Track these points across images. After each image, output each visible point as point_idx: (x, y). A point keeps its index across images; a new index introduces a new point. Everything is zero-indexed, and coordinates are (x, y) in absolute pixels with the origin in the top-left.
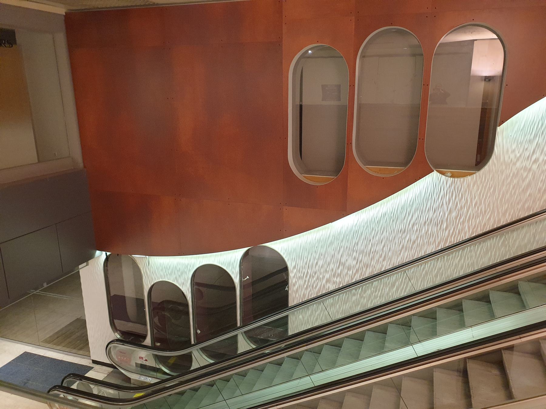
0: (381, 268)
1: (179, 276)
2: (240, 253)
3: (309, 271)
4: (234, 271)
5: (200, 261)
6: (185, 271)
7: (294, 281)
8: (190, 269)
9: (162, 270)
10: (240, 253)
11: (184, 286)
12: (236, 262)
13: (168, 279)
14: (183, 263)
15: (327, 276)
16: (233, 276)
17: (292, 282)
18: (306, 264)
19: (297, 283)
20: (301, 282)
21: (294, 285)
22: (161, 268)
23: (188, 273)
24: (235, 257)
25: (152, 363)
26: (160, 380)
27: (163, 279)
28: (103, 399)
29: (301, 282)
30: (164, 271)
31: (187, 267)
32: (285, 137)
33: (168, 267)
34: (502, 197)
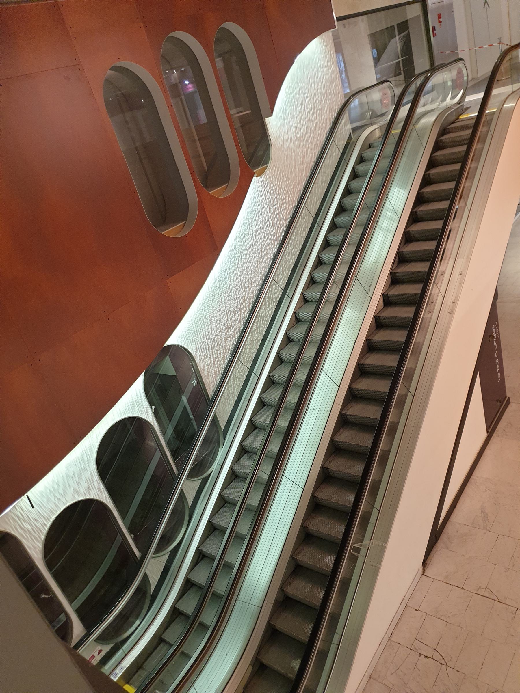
0: (289, 219)
1: (78, 483)
2: (139, 384)
3: (209, 343)
4: (142, 409)
5: (97, 435)
6: (83, 467)
7: (202, 366)
8: (88, 457)
9: (48, 500)
10: (139, 384)
11: (90, 491)
12: (139, 397)
13: (64, 504)
14: (75, 459)
15: (223, 335)
16: (105, 501)
17: (201, 368)
18: (204, 337)
19: (206, 366)
20: (208, 361)
21: (204, 370)
22: (49, 491)
23: (88, 468)
24: (132, 397)
25: (164, 558)
26: (410, 104)
27: (57, 512)
28: (287, 437)
29: (208, 361)
30: (52, 499)
31: (83, 459)
32: (105, 310)
33: (56, 487)
34: (288, 179)
